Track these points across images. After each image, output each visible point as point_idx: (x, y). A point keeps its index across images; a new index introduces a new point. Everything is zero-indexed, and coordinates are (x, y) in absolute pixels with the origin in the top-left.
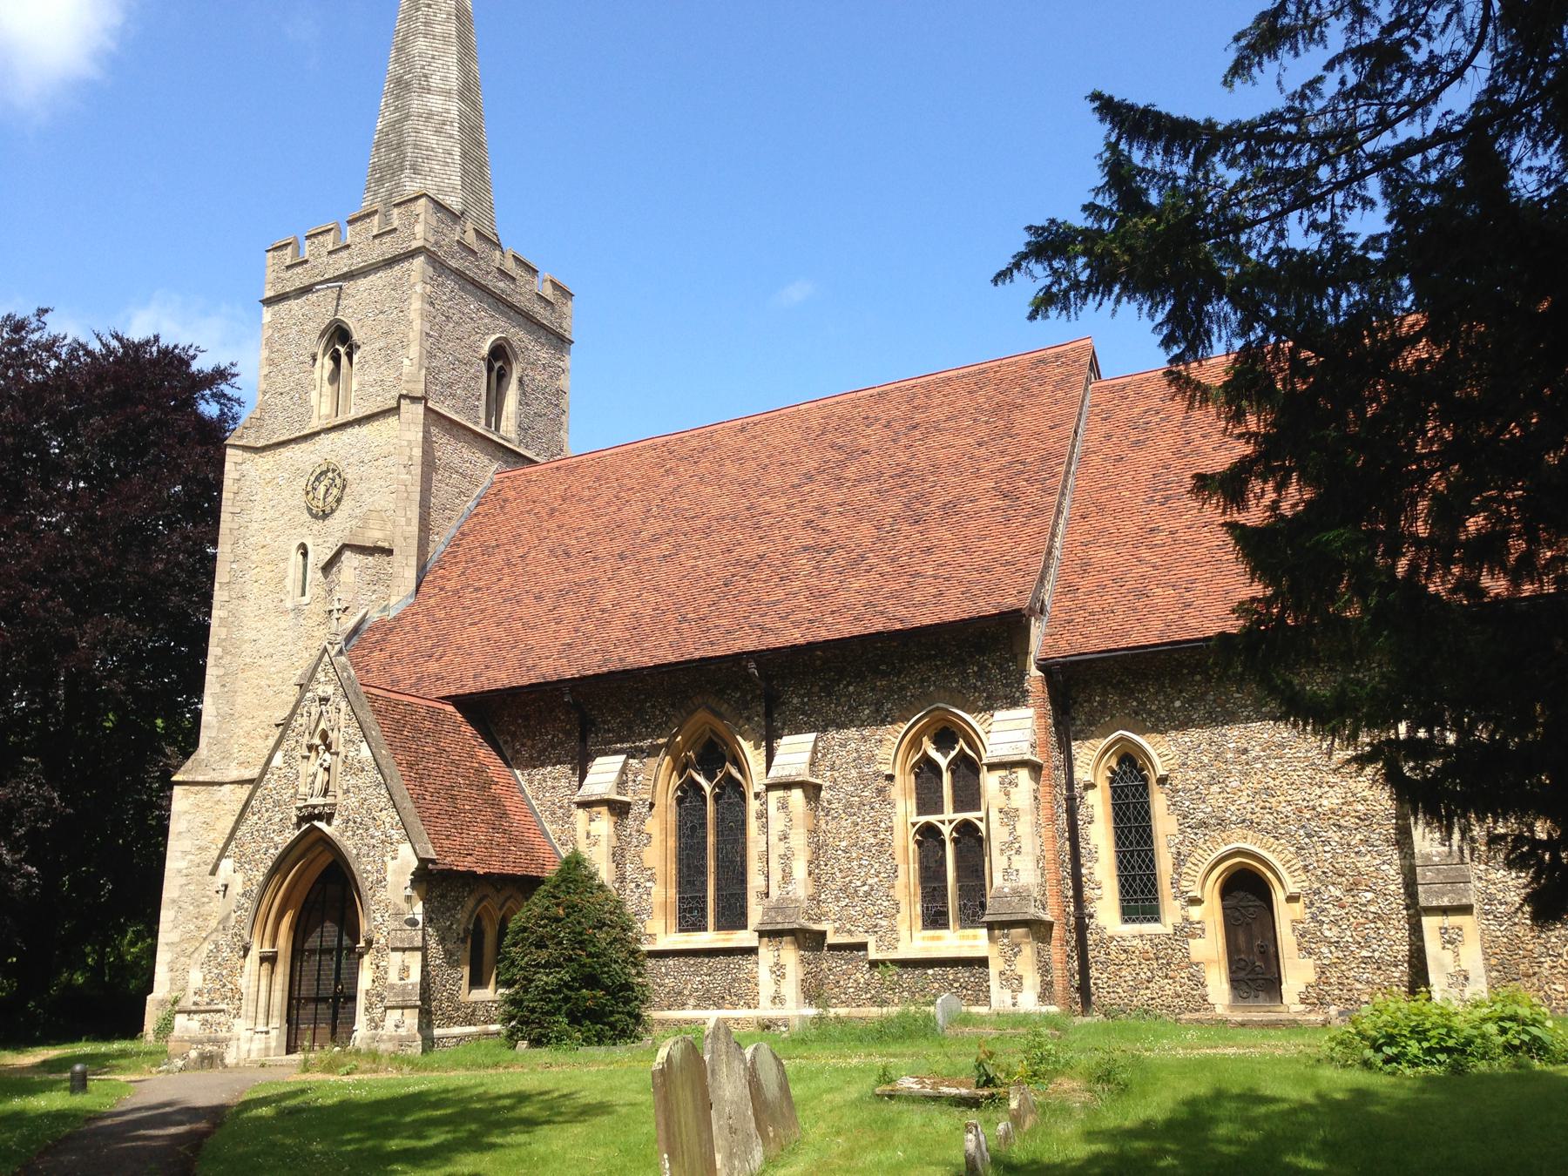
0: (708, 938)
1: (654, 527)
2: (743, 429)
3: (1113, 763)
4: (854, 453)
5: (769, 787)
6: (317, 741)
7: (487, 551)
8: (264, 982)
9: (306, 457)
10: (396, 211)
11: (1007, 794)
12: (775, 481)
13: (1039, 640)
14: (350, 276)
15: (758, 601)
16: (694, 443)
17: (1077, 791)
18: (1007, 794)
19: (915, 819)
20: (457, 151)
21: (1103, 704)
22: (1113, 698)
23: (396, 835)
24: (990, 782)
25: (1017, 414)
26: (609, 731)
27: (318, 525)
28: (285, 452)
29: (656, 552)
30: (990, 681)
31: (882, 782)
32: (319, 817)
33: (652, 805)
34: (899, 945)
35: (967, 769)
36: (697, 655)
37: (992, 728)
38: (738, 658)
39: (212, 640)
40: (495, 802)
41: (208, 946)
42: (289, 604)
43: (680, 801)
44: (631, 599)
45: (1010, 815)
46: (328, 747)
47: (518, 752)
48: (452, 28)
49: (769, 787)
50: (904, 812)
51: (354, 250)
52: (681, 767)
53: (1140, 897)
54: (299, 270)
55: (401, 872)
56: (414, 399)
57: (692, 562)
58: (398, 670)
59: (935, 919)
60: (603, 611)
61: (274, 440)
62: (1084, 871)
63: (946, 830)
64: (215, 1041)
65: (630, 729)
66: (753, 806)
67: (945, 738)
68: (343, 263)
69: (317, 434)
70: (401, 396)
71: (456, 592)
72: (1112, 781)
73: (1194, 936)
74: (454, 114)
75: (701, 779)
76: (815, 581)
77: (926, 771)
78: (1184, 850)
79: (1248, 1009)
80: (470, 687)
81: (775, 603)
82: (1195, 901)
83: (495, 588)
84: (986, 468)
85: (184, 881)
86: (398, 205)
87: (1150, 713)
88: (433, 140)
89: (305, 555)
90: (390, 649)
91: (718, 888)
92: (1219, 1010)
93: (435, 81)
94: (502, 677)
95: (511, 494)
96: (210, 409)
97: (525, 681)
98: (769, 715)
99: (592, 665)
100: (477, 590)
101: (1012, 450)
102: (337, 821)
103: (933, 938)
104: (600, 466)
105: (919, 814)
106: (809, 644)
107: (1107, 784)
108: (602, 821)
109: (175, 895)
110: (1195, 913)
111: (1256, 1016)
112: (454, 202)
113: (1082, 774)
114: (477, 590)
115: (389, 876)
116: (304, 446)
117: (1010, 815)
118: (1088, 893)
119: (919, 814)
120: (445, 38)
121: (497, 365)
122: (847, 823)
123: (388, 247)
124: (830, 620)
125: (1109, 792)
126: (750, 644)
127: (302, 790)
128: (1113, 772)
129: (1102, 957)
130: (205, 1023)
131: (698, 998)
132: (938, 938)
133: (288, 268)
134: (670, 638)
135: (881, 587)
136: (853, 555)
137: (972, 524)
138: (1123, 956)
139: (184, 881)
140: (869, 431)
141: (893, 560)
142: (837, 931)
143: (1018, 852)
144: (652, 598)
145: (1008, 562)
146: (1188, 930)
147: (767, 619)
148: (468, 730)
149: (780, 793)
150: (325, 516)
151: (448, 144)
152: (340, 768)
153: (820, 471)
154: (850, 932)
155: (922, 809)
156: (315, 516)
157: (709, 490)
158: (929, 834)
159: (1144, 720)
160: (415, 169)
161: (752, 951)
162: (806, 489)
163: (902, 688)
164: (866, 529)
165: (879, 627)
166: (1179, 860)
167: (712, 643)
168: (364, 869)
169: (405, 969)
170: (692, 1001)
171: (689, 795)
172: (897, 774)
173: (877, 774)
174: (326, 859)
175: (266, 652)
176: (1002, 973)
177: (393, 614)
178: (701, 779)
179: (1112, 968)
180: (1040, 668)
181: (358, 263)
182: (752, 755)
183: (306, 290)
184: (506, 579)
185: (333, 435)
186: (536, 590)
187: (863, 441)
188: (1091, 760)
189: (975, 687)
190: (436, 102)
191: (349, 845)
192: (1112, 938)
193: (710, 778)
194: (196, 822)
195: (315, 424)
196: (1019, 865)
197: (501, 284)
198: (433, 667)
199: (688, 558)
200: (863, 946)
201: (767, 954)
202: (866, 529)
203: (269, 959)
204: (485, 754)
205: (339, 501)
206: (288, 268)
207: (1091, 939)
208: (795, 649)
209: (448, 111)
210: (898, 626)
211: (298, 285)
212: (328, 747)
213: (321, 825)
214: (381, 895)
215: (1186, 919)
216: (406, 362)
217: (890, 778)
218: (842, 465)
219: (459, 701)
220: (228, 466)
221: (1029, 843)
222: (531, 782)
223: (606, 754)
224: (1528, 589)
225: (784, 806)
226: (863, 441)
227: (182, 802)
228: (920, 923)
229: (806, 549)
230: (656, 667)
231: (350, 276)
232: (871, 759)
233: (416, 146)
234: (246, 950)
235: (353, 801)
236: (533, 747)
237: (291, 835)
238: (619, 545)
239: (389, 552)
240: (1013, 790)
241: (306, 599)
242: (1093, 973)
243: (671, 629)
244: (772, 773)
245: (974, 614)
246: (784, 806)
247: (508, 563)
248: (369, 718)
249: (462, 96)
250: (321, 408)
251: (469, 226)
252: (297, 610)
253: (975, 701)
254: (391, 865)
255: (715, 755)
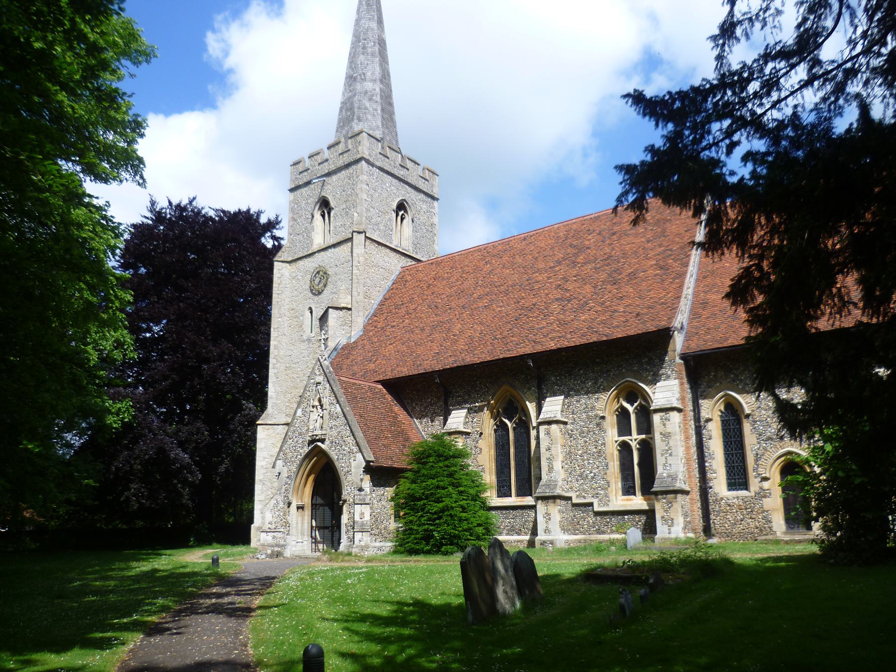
0: (513, 500)
1: (480, 291)
2: (525, 239)
3: (722, 408)
4: (581, 249)
5: (540, 424)
6: (317, 403)
7: (397, 307)
8: (300, 521)
9: (310, 265)
10: (350, 141)
11: (664, 425)
12: (541, 265)
13: (678, 342)
14: (329, 174)
15: (532, 328)
16: (500, 247)
17: (702, 423)
18: (664, 425)
19: (616, 438)
20: (379, 108)
21: (715, 376)
22: (721, 373)
23: (355, 449)
24: (656, 418)
25: (668, 225)
26: (459, 396)
27: (316, 298)
28: (301, 263)
29: (480, 304)
30: (655, 366)
31: (598, 420)
32: (319, 440)
33: (481, 434)
34: (610, 503)
35: (645, 414)
36: (501, 356)
37: (657, 390)
38: (523, 358)
39: (271, 356)
40: (402, 432)
41: (273, 502)
42: (305, 338)
43: (495, 431)
44: (469, 329)
45: (666, 436)
46: (322, 406)
47: (414, 408)
48: (377, 48)
49: (540, 424)
50: (612, 435)
51: (331, 162)
52: (495, 416)
53: (738, 477)
54: (306, 173)
55: (357, 467)
56: (359, 233)
57: (499, 309)
58: (355, 368)
59: (628, 490)
60: (454, 335)
61: (296, 257)
62: (707, 464)
63: (634, 445)
64: (277, 545)
65: (469, 395)
66: (533, 433)
67: (632, 394)
68: (326, 168)
69: (315, 253)
70: (354, 231)
71: (382, 328)
72: (721, 416)
73: (765, 497)
74: (378, 90)
75: (506, 421)
76: (562, 316)
77: (623, 415)
78: (759, 452)
79: (793, 534)
80: (389, 376)
81: (542, 328)
82: (765, 479)
83: (401, 325)
84: (651, 254)
85: (265, 471)
86: (351, 138)
87: (741, 381)
88: (368, 105)
89: (311, 312)
90: (352, 357)
91: (517, 475)
92: (779, 534)
93: (369, 74)
94: (405, 371)
95: (409, 278)
96: (269, 243)
97: (416, 372)
98: (539, 388)
99: (449, 362)
100: (393, 327)
101: (665, 244)
102: (327, 442)
103: (627, 500)
104: (561, 395)
105: (619, 436)
106: (559, 349)
107: (719, 419)
108: (470, 429)
109: (261, 478)
110: (766, 485)
111: (797, 537)
112: (378, 134)
113: (704, 414)
114: (393, 327)
115: (352, 469)
116: (309, 259)
117: (666, 436)
118: (709, 475)
119: (619, 436)
120: (373, 55)
121: (401, 213)
122: (581, 442)
123: (347, 159)
124: (569, 336)
125: (720, 423)
126: (528, 350)
127: (311, 427)
128: (722, 412)
129: (717, 508)
130: (274, 537)
131: (508, 530)
132: (630, 500)
133: (301, 173)
134: (488, 348)
135: (596, 318)
136: (581, 302)
137: (644, 284)
138: (728, 508)
139: (265, 471)
140: (590, 237)
141: (602, 304)
142: (577, 496)
143: (671, 455)
144: (479, 328)
145: (663, 303)
146: (763, 494)
147: (537, 337)
148: (389, 397)
149: (546, 427)
150: (320, 293)
151: (375, 106)
152: (328, 417)
153: (564, 259)
154: (584, 497)
155: (620, 434)
156: (314, 294)
157: (508, 271)
158: (625, 448)
159: (738, 385)
160: (359, 120)
161: (533, 507)
162: (557, 268)
163: (608, 371)
164: (588, 288)
165: (595, 339)
166: (757, 458)
167: (509, 350)
168: (341, 465)
169: (362, 514)
170: (505, 531)
171: (501, 429)
172: (606, 415)
173: (596, 416)
174: (324, 461)
175: (296, 361)
176: (663, 517)
177: (353, 340)
178: (506, 421)
179: (722, 514)
180: (681, 358)
181: (332, 167)
182: (531, 407)
183: (308, 183)
184: (407, 321)
185: (322, 253)
186: (421, 325)
187: (587, 243)
188: (712, 409)
189: (647, 369)
190: (368, 85)
191: (333, 455)
192: (722, 499)
193: (510, 421)
194: (268, 442)
195: (315, 248)
196: (674, 463)
197: (402, 173)
198: (372, 366)
199: (497, 307)
200: (591, 504)
201: (541, 507)
202: (588, 288)
203: (300, 508)
204: (397, 409)
205: (325, 286)
206: (301, 173)
207: (711, 499)
208: (552, 352)
209: (375, 90)
210: (605, 339)
211: (305, 180)
212: (322, 406)
213: (319, 444)
214: (349, 478)
215: (761, 488)
216: (356, 214)
217: (603, 418)
218: (576, 255)
219: (386, 384)
220: (275, 271)
221: (680, 451)
222: (421, 423)
223: (458, 409)
224: (874, 321)
225: (548, 433)
226: (587, 243)
227: (262, 433)
228: (620, 492)
229: (557, 300)
230: (481, 363)
231: (329, 174)
232: (593, 408)
233: (359, 108)
234: (289, 504)
235: (334, 433)
236: (421, 405)
237: (306, 449)
238: (463, 301)
239: (350, 309)
240: (667, 423)
241: (313, 335)
242: (712, 517)
243: (488, 343)
244: (541, 417)
245: (644, 331)
246: (548, 433)
247: (408, 313)
248: (340, 392)
249: (381, 81)
250: (318, 241)
251: (386, 144)
252: (309, 340)
253: (647, 377)
254: (353, 464)
255: (512, 409)
